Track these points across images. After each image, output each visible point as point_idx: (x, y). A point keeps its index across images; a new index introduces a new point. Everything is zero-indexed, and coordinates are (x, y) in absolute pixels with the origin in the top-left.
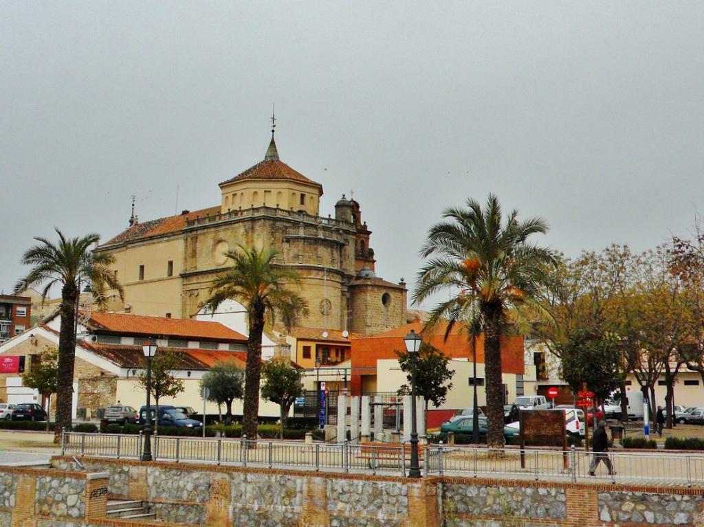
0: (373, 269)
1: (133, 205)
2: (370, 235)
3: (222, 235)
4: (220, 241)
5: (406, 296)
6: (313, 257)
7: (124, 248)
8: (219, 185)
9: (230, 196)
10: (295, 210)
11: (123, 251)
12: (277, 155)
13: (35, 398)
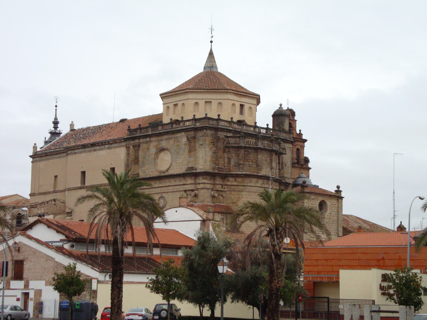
0: (308, 176)
1: (56, 106)
2: (306, 144)
3: (164, 144)
4: (162, 150)
5: (342, 202)
6: (253, 166)
7: (65, 154)
8: (161, 95)
9: (171, 106)
10: (235, 120)
11: (63, 157)
12: (216, 65)
13: (18, 300)
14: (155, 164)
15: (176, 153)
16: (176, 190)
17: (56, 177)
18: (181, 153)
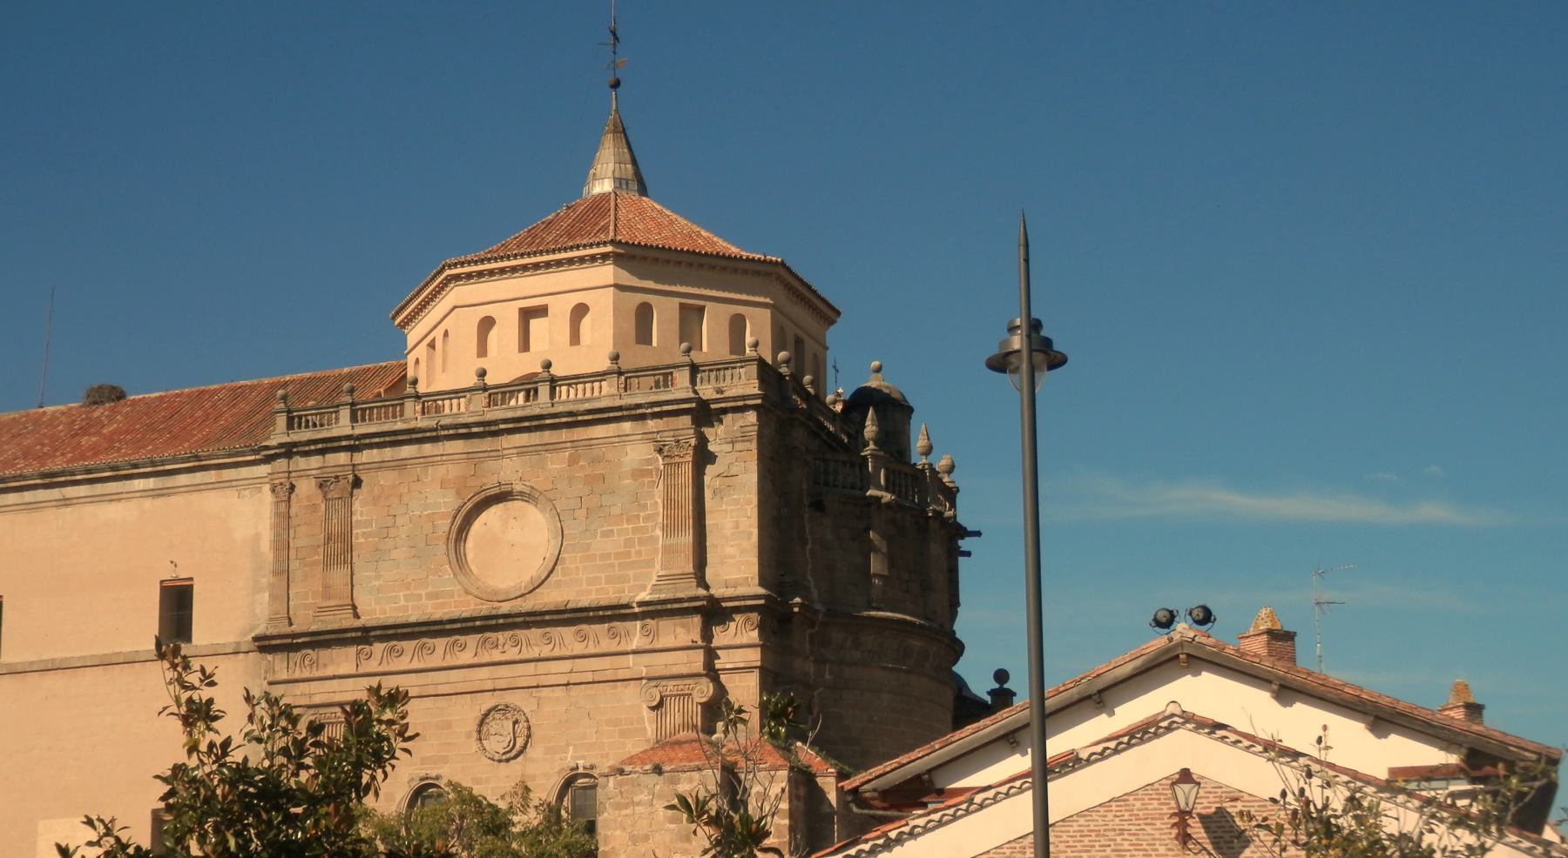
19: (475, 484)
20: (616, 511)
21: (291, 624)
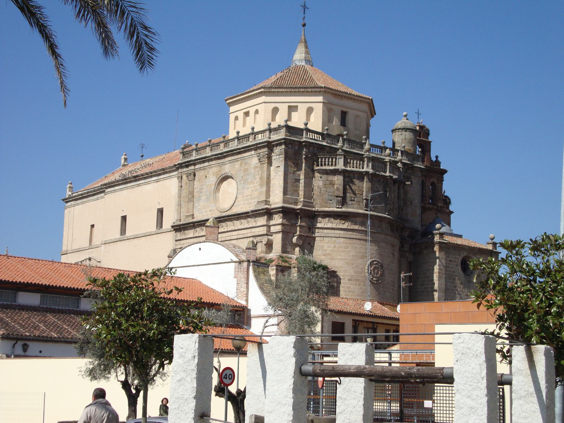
4: (225, 178)
7: (103, 195)
14: (216, 199)
15: (242, 181)
16: (241, 236)
17: (93, 226)
18: (250, 180)
19: (220, 174)
20: (250, 180)
21: (193, 218)
